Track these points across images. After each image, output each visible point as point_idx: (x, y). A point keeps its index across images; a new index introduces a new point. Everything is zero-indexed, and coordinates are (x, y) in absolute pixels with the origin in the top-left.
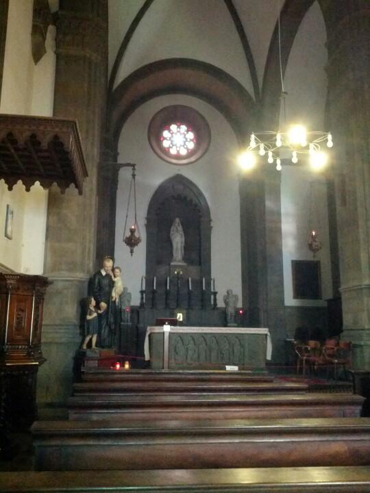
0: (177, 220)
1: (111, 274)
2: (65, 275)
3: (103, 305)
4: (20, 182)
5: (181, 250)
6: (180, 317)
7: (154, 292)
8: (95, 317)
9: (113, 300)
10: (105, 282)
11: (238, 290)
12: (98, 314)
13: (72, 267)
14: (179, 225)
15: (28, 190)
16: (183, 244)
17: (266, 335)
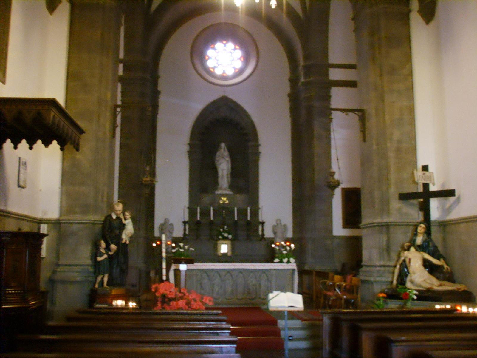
0: (223, 145)
1: (122, 216)
2: (78, 217)
3: (113, 247)
4: (24, 141)
5: (228, 177)
6: (224, 248)
7: (198, 223)
8: (105, 258)
9: (123, 242)
10: (116, 224)
11: (288, 219)
12: (108, 255)
13: (86, 209)
14: (224, 150)
15: (31, 148)
16: (230, 170)
17: (293, 270)
